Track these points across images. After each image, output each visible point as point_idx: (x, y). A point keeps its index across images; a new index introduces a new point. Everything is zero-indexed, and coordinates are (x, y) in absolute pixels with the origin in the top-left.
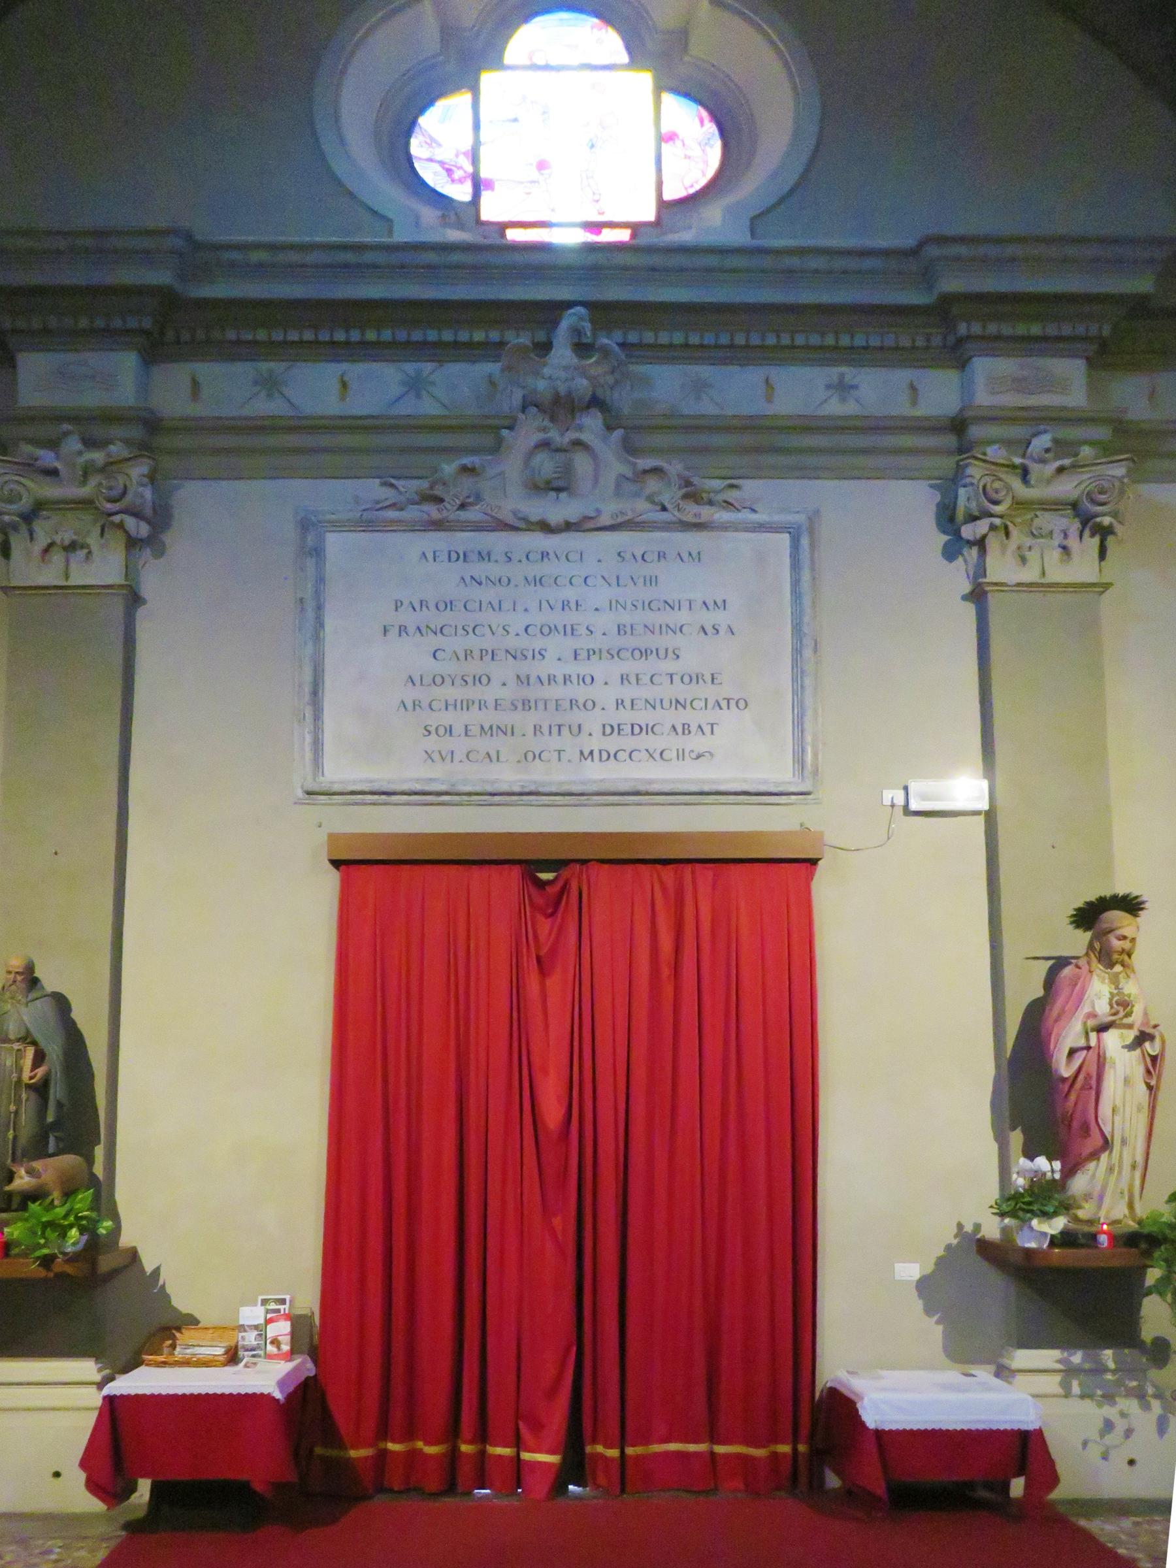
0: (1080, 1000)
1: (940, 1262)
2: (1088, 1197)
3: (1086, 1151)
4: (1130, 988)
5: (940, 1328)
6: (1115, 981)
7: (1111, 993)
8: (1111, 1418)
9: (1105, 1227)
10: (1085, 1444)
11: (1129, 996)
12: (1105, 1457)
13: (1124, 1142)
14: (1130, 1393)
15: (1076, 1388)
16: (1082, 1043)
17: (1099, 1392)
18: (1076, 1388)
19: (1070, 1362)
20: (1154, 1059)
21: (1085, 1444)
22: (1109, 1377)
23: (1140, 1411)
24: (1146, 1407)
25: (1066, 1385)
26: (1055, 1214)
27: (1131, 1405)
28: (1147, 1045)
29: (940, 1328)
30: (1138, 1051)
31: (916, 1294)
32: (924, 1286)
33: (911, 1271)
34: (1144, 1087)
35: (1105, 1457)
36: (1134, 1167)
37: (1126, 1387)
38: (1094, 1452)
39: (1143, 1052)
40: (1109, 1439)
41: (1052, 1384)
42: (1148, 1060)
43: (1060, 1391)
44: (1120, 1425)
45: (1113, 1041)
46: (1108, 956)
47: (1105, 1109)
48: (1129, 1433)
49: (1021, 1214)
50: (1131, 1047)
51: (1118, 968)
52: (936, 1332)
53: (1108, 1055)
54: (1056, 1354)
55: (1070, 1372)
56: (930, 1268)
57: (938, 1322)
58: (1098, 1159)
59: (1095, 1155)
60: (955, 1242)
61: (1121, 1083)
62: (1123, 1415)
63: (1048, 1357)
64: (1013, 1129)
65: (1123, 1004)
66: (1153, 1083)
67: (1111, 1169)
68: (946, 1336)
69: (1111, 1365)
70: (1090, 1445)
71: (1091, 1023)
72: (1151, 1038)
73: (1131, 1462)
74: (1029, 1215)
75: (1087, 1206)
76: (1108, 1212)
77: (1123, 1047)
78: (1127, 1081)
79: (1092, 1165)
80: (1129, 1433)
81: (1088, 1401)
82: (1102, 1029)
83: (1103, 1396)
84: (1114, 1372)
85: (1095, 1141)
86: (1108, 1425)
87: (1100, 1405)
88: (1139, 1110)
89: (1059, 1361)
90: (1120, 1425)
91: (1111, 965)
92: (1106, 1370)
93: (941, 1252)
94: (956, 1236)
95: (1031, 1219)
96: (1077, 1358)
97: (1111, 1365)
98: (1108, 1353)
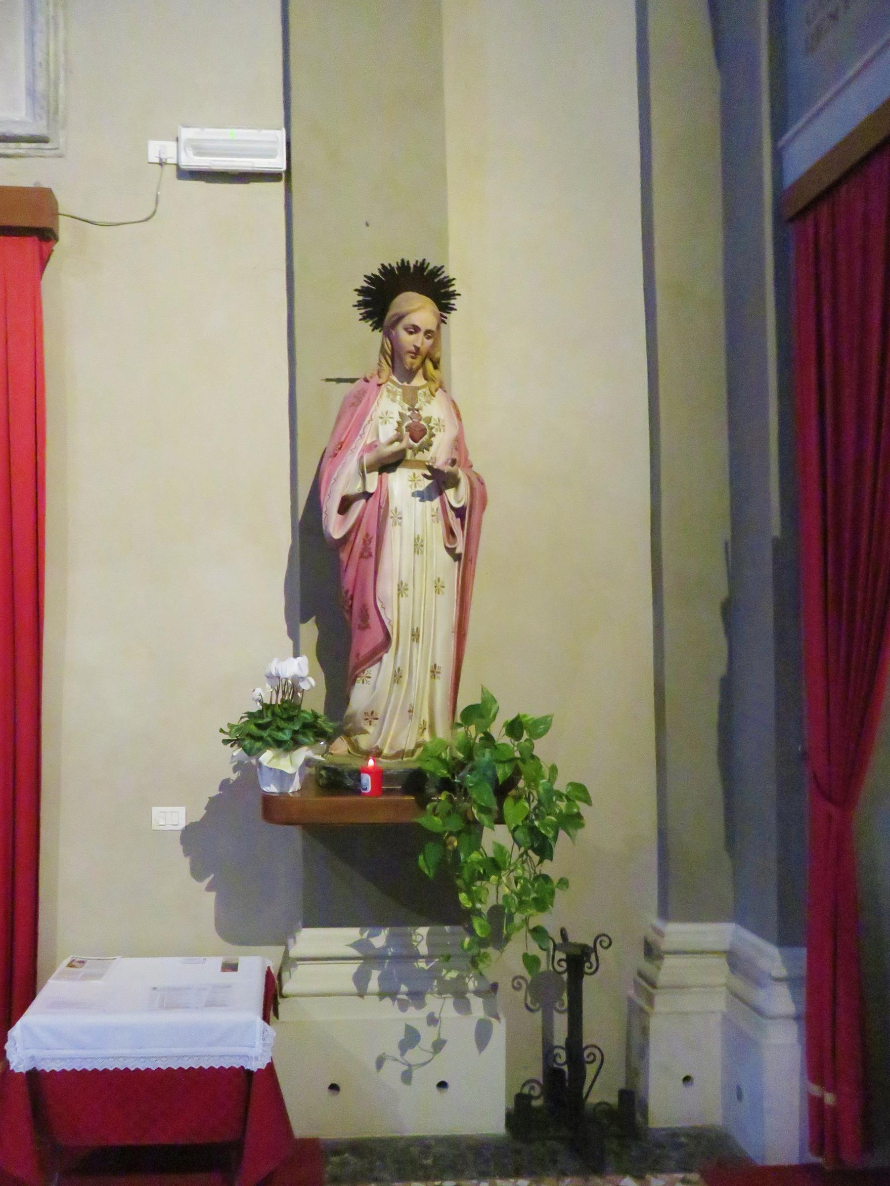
0: (359, 425)
1: (214, 804)
2: (371, 716)
3: (365, 651)
4: (433, 409)
5: (213, 895)
6: (411, 398)
7: (401, 415)
8: (415, 1025)
9: (371, 763)
10: (380, 1063)
11: (429, 420)
12: (407, 1077)
13: (415, 636)
14: (446, 988)
15: (374, 985)
16: (357, 488)
17: (404, 988)
18: (374, 985)
19: (371, 946)
20: (460, 513)
21: (380, 1063)
22: (422, 964)
23: (455, 1014)
24: (463, 1005)
25: (361, 979)
26: (296, 744)
27: (439, 1004)
28: (450, 493)
29: (213, 895)
30: (436, 502)
31: (180, 848)
32: (191, 836)
33: (173, 818)
34: (448, 558)
35: (407, 1077)
36: (434, 672)
37: (441, 980)
38: (393, 1071)
39: (443, 503)
40: (414, 1055)
41: (344, 975)
42: (451, 514)
43: (352, 987)
44: (428, 1035)
45: (402, 484)
46: (413, 364)
47: (387, 588)
48: (438, 1045)
49: (247, 742)
50: (424, 496)
51: (418, 381)
52: (207, 902)
53: (392, 507)
54: (353, 933)
55: (369, 958)
56: (199, 813)
57: (209, 888)
58: (380, 659)
59: (375, 656)
60: (234, 777)
61: (409, 547)
62: (432, 1020)
63: (341, 939)
64: (304, 620)
65: (419, 433)
66: (460, 549)
67: (397, 677)
68: (222, 904)
69: (423, 949)
70: (387, 1064)
71: (368, 458)
72: (454, 482)
73: (442, 1085)
74: (258, 744)
75: (371, 729)
76: (394, 739)
77: (413, 495)
78: (418, 545)
79: (373, 671)
80: (438, 1045)
81: (387, 1001)
82: (389, 465)
83: (409, 994)
84: (429, 958)
85: (374, 636)
86: (411, 1038)
87: (403, 1007)
88: (438, 588)
89: (356, 945)
90: (428, 1035)
91: (409, 375)
92: (417, 957)
93: (215, 791)
94: (235, 769)
95: (260, 751)
96: (380, 940)
97: (423, 949)
98: (423, 931)
